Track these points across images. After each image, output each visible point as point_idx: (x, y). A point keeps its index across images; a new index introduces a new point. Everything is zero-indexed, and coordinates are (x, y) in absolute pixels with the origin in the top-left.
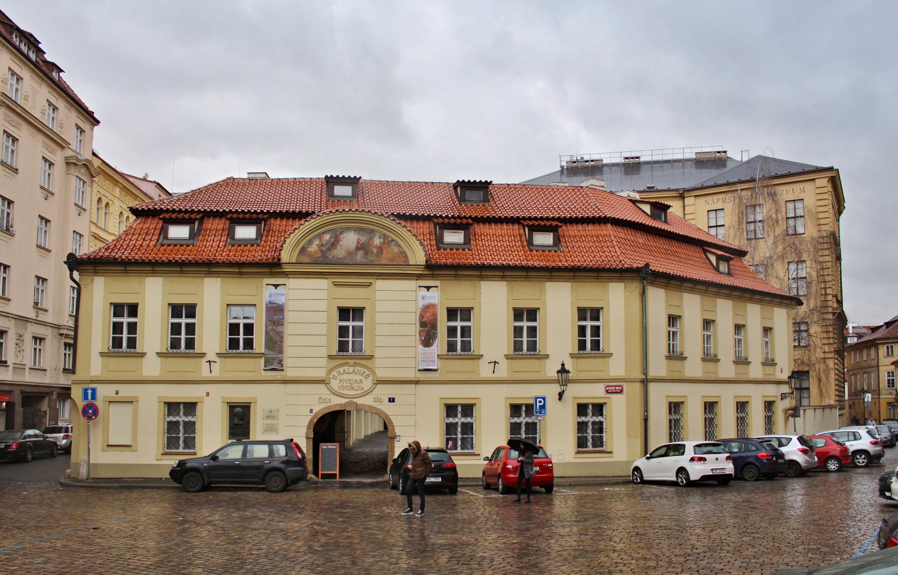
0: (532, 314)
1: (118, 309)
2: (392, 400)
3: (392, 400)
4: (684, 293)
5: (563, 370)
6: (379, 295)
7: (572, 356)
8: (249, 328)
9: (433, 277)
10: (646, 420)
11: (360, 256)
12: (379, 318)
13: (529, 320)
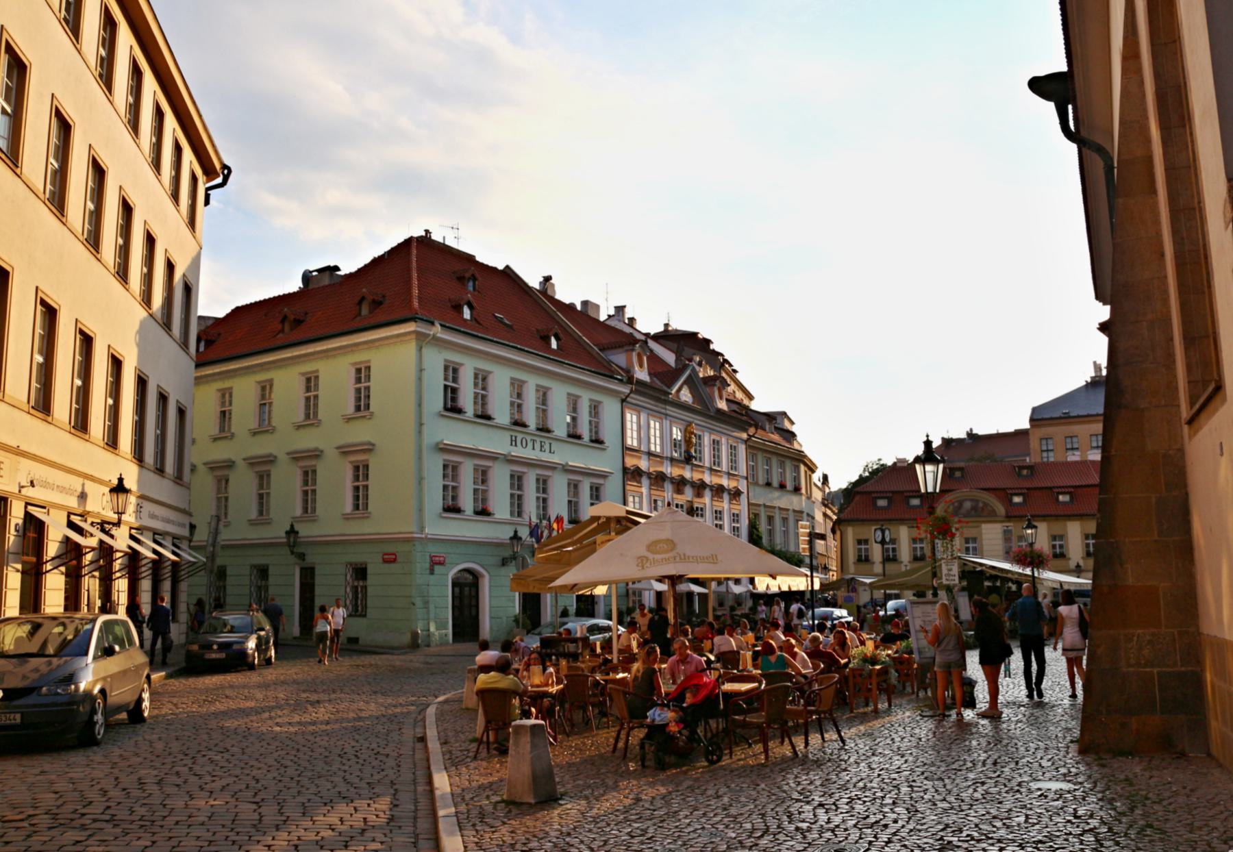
0: (975, 540)
1: (859, 542)
4: (984, 526)
5: (1078, 566)
6: (984, 531)
7: (1083, 558)
9: (1009, 521)
11: (973, 513)
12: (984, 542)
13: (865, 544)
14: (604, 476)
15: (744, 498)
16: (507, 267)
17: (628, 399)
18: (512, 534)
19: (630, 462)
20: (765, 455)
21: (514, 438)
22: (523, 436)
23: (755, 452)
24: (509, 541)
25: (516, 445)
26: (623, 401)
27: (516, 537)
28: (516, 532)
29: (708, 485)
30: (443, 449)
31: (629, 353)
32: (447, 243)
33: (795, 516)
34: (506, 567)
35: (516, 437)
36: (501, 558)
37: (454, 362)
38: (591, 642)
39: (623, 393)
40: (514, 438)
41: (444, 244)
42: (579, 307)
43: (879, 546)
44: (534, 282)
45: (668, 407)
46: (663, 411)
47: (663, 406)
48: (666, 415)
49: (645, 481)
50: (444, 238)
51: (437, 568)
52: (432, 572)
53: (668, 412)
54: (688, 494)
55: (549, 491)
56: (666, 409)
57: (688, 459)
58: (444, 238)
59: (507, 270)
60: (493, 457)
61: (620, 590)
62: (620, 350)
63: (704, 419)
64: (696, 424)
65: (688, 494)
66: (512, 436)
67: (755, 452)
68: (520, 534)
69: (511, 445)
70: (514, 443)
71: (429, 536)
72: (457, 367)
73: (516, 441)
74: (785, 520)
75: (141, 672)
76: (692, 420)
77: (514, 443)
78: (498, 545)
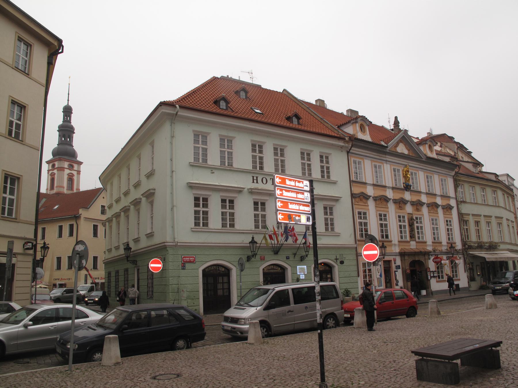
2: (103, 198)
3: (103, 198)
8: (404, 217)
10: (69, 94)
14: (336, 200)
15: (455, 212)
16: (284, 90)
17: (351, 151)
18: (250, 240)
19: (357, 190)
20: (469, 185)
21: (255, 178)
22: (263, 176)
23: (496, 189)
24: (249, 245)
25: (257, 182)
26: (348, 152)
27: (253, 242)
28: (253, 238)
29: (424, 203)
30: (191, 186)
31: (355, 124)
32: (241, 79)
33: (445, 217)
34: (249, 262)
35: (257, 177)
36: (246, 256)
37: (259, 142)
38: (362, 306)
39: (347, 147)
40: (255, 178)
41: (239, 80)
42: (345, 113)
43: (386, 257)
44: (389, 126)
45: (387, 156)
46: (385, 159)
47: (384, 156)
48: (386, 161)
49: (425, 206)
50: (239, 77)
51: (187, 265)
52: (183, 268)
53: (387, 159)
54: (409, 209)
55: (334, 214)
56: (386, 157)
57: (407, 188)
58: (239, 77)
59: (285, 92)
60: (239, 191)
61: (101, 310)
62: (350, 124)
63: (419, 164)
64: (409, 166)
65: (409, 209)
66: (253, 177)
67: (496, 189)
68: (255, 240)
69: (253, 182)
70: (255, 181)
71: (179, 244)
72: (262, 144)
73: (257, 180)
74: (477, 223)
75: (306, 290)
76: (406, 164)
77: (255, 181)
78: (243, 248)
